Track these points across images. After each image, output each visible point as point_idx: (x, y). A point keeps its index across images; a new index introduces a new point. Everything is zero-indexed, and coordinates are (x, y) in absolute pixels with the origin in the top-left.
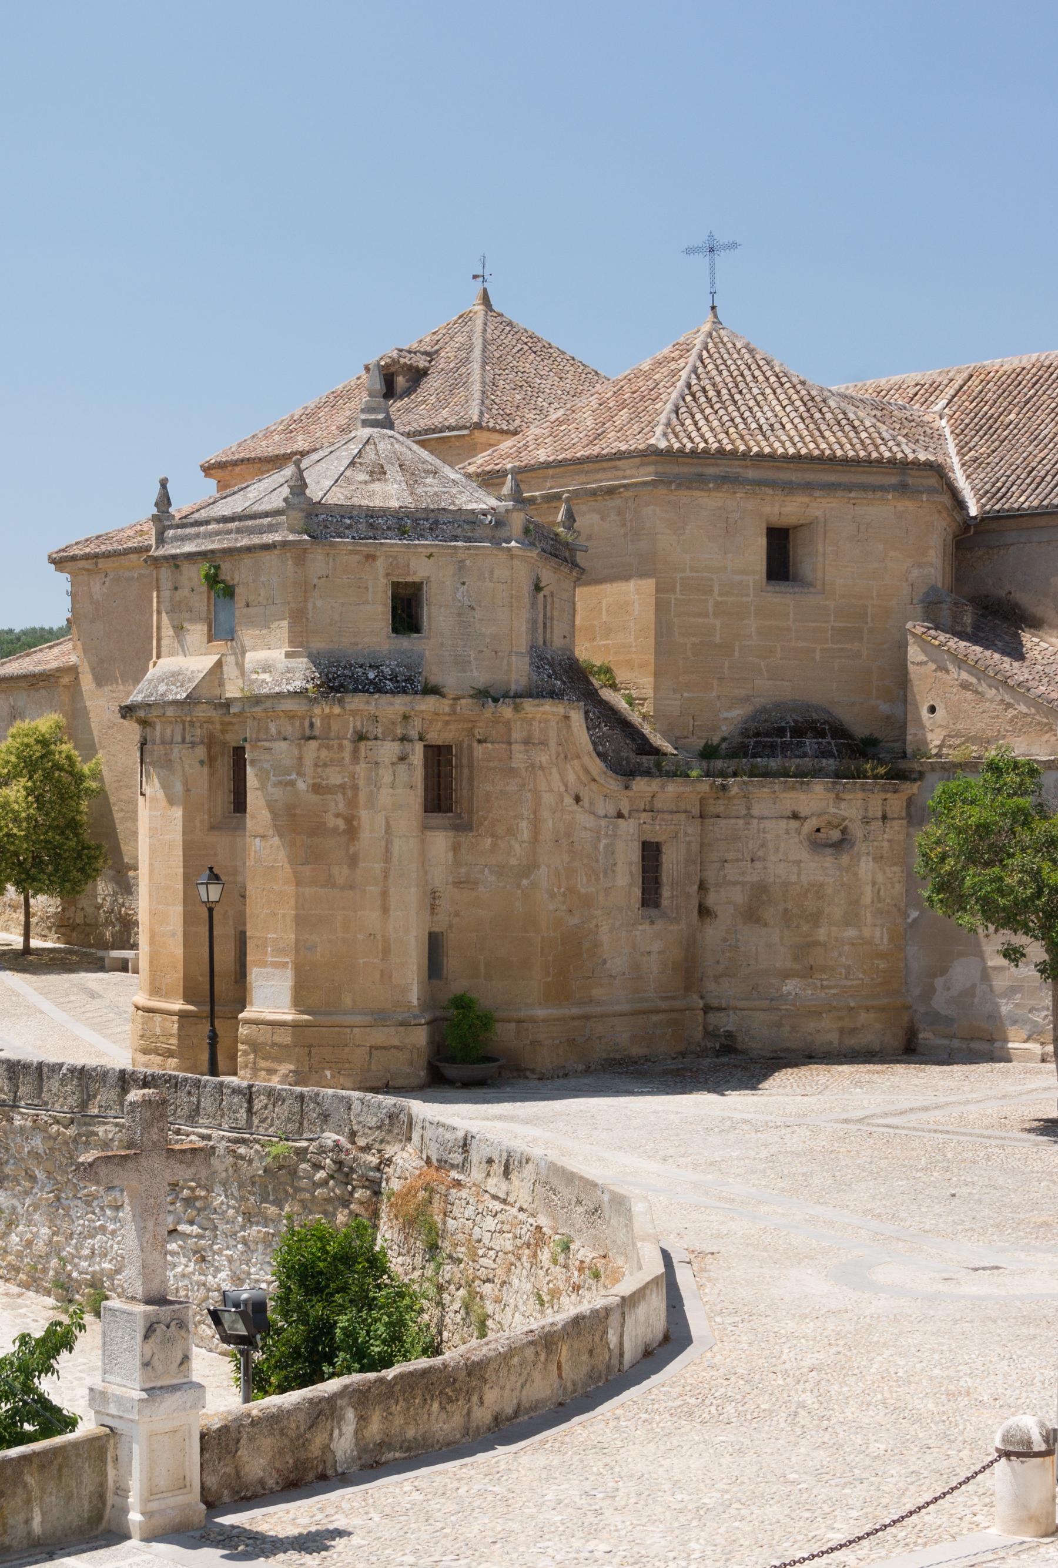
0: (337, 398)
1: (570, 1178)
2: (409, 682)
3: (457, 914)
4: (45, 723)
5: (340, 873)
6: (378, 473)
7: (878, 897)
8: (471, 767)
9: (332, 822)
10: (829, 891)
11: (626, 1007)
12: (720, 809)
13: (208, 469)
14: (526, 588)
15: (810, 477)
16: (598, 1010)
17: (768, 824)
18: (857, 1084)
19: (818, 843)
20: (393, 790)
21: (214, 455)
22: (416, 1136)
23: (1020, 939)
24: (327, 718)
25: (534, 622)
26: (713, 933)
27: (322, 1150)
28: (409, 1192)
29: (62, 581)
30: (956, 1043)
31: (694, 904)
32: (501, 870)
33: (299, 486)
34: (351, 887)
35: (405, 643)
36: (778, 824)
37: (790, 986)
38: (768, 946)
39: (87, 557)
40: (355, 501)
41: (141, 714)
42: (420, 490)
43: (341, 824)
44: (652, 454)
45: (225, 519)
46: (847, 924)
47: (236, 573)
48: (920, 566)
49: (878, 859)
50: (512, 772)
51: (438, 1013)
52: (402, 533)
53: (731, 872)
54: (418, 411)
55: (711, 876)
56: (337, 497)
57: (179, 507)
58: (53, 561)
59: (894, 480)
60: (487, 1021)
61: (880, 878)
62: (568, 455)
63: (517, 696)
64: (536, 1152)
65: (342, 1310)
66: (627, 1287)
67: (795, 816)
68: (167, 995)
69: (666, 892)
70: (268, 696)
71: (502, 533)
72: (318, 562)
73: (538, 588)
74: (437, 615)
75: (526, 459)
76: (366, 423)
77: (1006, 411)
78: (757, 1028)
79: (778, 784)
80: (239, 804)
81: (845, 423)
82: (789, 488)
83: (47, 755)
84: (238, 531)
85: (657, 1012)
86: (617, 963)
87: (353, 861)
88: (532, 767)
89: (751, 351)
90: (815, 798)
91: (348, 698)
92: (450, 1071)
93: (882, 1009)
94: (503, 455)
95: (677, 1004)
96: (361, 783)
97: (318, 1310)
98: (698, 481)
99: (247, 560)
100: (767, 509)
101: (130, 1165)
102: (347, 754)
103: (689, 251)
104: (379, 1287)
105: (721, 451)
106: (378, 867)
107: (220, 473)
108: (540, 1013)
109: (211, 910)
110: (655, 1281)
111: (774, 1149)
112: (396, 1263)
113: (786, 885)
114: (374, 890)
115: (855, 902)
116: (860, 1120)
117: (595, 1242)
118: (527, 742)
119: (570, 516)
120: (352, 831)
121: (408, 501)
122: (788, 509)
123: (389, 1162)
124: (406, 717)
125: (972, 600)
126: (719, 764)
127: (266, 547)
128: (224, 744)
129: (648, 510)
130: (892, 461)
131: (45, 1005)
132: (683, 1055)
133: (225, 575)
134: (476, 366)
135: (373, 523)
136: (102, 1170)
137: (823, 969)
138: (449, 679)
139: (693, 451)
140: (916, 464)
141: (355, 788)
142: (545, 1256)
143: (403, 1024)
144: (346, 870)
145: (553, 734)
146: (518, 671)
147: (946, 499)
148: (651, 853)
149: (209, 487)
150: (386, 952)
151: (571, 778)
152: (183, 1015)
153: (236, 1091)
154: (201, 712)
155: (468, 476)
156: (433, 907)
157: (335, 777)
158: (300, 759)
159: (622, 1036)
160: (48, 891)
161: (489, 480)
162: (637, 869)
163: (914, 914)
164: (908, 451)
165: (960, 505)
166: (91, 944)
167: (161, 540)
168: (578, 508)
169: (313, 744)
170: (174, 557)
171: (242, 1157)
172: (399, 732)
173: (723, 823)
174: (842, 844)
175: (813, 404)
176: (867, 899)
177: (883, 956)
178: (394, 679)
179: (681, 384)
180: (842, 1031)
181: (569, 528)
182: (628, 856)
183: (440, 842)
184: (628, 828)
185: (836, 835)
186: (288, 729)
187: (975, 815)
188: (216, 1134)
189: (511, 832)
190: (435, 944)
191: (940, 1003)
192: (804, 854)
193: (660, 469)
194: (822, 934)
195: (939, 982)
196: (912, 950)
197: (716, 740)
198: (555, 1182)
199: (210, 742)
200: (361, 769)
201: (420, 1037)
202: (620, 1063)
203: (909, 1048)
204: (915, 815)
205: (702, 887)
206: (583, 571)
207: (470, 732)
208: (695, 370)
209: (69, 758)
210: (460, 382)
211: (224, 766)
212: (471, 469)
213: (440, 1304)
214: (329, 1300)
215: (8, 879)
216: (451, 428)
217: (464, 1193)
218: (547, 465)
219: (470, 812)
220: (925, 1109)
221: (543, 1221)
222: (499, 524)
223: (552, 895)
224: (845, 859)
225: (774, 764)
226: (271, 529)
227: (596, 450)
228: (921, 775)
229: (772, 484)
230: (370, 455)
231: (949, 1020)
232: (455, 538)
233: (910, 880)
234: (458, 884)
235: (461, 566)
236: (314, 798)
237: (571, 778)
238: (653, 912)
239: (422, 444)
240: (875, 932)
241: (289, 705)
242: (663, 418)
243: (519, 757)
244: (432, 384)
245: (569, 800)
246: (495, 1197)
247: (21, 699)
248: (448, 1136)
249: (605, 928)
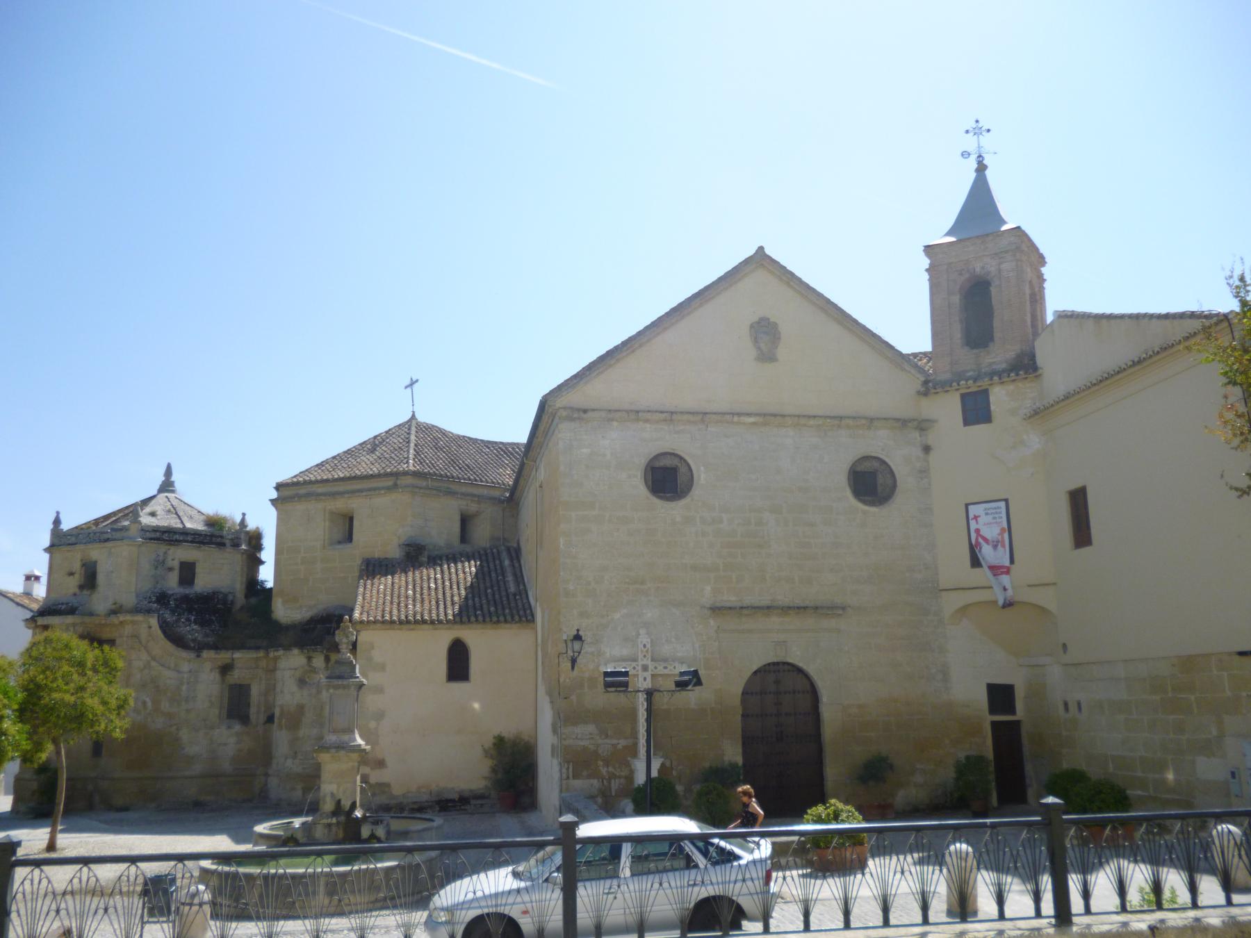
59: (390, 483)
82: (334, 495)
122: (340, 504)
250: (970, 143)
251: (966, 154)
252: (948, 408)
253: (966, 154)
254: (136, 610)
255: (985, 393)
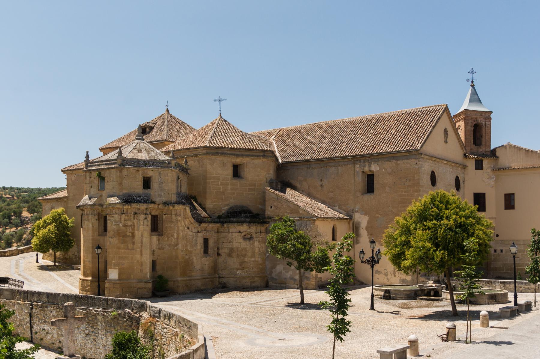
0: (132, 133)
1: (184, 320)
2: (147, 200)
3: (159, 256)
4: (60, 210)
5: (130, 246)
6: (140, 151)
7: (259, 251)
8: (162, 220)
9: (128, 234)
10: (248, 249)
11: (200, 277)
12: (222, 230)
13: (101, 150)
14: (176, 178)
15: (243, 153)
16: (193, 278)
17: (234, 234)
18: (254, 295)
19: (245, 238)
20: (143, 227)
21: (102, 146)
22: (148, 310)
23: (290, 260)
24: (127, 209)
25: (177, 187)
26: (221, 260)
27: (125, 314)
28: (146, 323)
29: (64, 176)
30: (277, 285)
31: (216, 252)
32: (170, 245)
33: (120, 153)
34: (133, 250)
35: (146, 191)
36: (235, 235)
37: (239, 272)
38: (234, 262)
39: (70, 170)
40: (134, 157)
41: (82, 208)
42: (150, 155)
43: (130, 234)
44: (206, 147)
45: (102, 161)
46: (252, 257)
47: (106, 174)
48: (268, 174)
49: (259, 242)
50: (172, 222)
51: (155, 280)
52: (146, 165)
53: (225, 245)
54: (153, 136)
55: (220, 246)
56: (130, 156)
57: (91, 159)
58: (62, 171)
59: (262, 154)
60: (166, 281)
61: (260, 246)
62: (186, 147)
63: (173, 204)
64: (176, 313)
65: (129, 353)
66: (194, 347)
67: (240, 232)
68: (87, 276)
69: (209, 250)
70: (113, 204)
71: (170, 165)
72: (125, 172)
73: (178, 178)
74: (154, 185)
75: (176, 148)
76: (137, 139)
77: (288, 139)
78: (231, 281)
79: (236, 225)
80: (106, 230)
81: (251, 141)
82: (238, 156)
83: (60, 218)
84: (106, 164)
85: (207, 278)
86: (198, 267)
87: (134, 243)
88: (177, 221)
89: (229, 124)
90: (244, 228)
91: (132, 204)
92: (158, 293)
93: (260, 277)
94: (171, 147)
95: (212, 276)
96: (136, 224)
97: (123, 353)
98: (217, 154)
99: (108, 171)
100: (233, 161)
101: (65, 322)
102: (132, 218)
103: (215, 101)
104: (138, 347)
105: (222, 147)
106: (140, 244)
107: (104, 151)
108: (179, 279)
109: (98, 255)
110: (202, 345)
111: (234, 311)
112: (142, 341)
113: (238, 248)
114: (139, 250)
115: (254, 252)
116: (255, 304)
117: (190, 335)
118: (176, 215)
119: (186, 162)
120: (133, 236)
121: (147, 158)
122: (238, 160)
123: (141, 316)
124: (146, 209)
125: (280, 182)
126: (222, 220)
127: (112, 168)
128: (102, 215)
129: (205, 161)
130: (262, 150)
131: (59, 279)
132: (214, 288)
133: (102, 175)
134: (165, 127)
135: (138, 163)
136: (57, 323)
137: (247, 268)
138: (157, 200)
139: (215, 147)
140: (267, 150)
141: (134, 226)
142: (178, 339)
143: (146, 282)
144: (132, 245)
145: (182, 213)
146: (174, 198)
147: (274, 159)
148: (206, 241)
149: (101, 154)
150: (142, 265)
151: (187, 223)
152: (90, 281)
153: (104, 299)
154: (97, 207)
155: (162, 152)
156: (153, 254)
157: (129, 223)
158: (121, 219)
159: (199, 284)
160: (61, 251)
161: (167, 153)
162: (202, 245)
163: (268, 255)
164: (265, 147)
165: (277, 160)
166: (67, 264)
167: (87, 166)
168: (189, 159)
169: (124, 215)
170: (90, 170)
171: (105, 316)
172: (145, 212)
173: (223, 234)
174: (251, 239)
175: (243, 136)
176: (257, 251)
177: (260, 264)
178: (144, 200)
179: (213, 131)
180: (251, 282)
181: (186, 164)
182: (200, 241)
183: (155, 239)
184: (200, 235)
185: (249, 236)
186: (118, 212)
187: (280, 232)
188: (99, 310)
189: (172, 236)
190: (154, 263)
191: (274, 275)
192: (242, 241)
193: (208, 151)
194: (246, 259)
195: (273, 270)
196: (267, 263)
197: (221, 214)
198: (180, 320)
199: (99, 215)
200: (135, 221)
201: (150, 285)
202: (198, 291)
203: (267, 286)
204: (267, 232)
205: (218, 249)
206: (189, 174)
207: (162, 212)
208: (216, 128)
209: (65, 218)
210: (161, 130)
211: (102, 220)
212: (163, 150)
213: (153, 351)
214: (125, 350)
215: (50, 248)
216: (159, 141)
217: (159, 323)
218: (181, 150)
219: (162, 231)
220: (270, 300)
221: (178, 330)
222: (169, 163)
223: (182, 251)
224: (251, 242)
225: (235, 220)
226: (114, 164)
227: (193, 146)
228: (269, 222)
229: (234, 155)
230: (138, 147)
231: (276, 279)
232: (159, 166)
233: (267, 247)
234: (159, 248)
235: (160, 173)
236: (124, 228)
237: (187, 223)
238: (206, 255)
239: (152, 145)
240: (259, 259)
241: (118, 206)
242: (208, 139)
243: (174, 218)
244: (155, 130)
245: (186, 228)
246: (166, 324)
247: (54, 204)
248: (155, 309)
249: (195, 259)
250: (469, 76)
251: (468, 80)
252: (471, 164)
253: (468, 80)
254: (178, 203)
255: (482, 161)
